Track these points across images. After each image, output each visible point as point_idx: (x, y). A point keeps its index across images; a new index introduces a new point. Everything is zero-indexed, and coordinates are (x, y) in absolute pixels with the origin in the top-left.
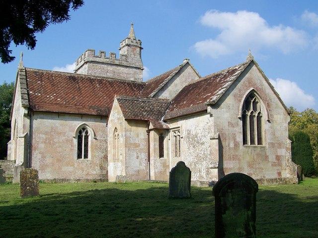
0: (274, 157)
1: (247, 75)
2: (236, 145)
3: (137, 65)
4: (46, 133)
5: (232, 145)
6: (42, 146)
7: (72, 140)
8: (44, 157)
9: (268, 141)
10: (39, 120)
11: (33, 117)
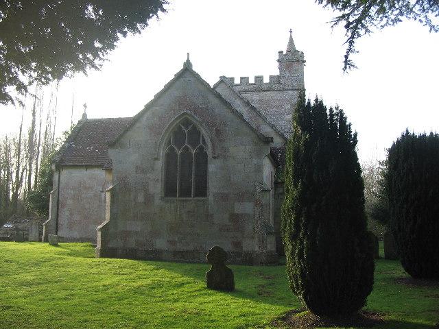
7: (100, 195)
8: (72, 214)
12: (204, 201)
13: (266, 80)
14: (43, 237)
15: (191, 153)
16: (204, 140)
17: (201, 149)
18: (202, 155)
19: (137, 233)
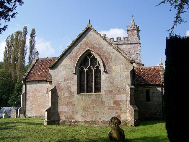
0: (112, 102)
1: (84, 40)
2: (71, 94)
3: (136, 41)
4: (33, 92)
5: (67, 94)
6: (31, 99)
7: (45, 95)
8: (32, 104)
9: (105, 89)
10: (29, 85)
11: (27, 84)
12: (100, 94)
13: (122, 39)
14: (18, 116)
15: (92, 70)
16: (99, 64)
17: (98, 67)
18: (98, 71)
19: (65, 112)
